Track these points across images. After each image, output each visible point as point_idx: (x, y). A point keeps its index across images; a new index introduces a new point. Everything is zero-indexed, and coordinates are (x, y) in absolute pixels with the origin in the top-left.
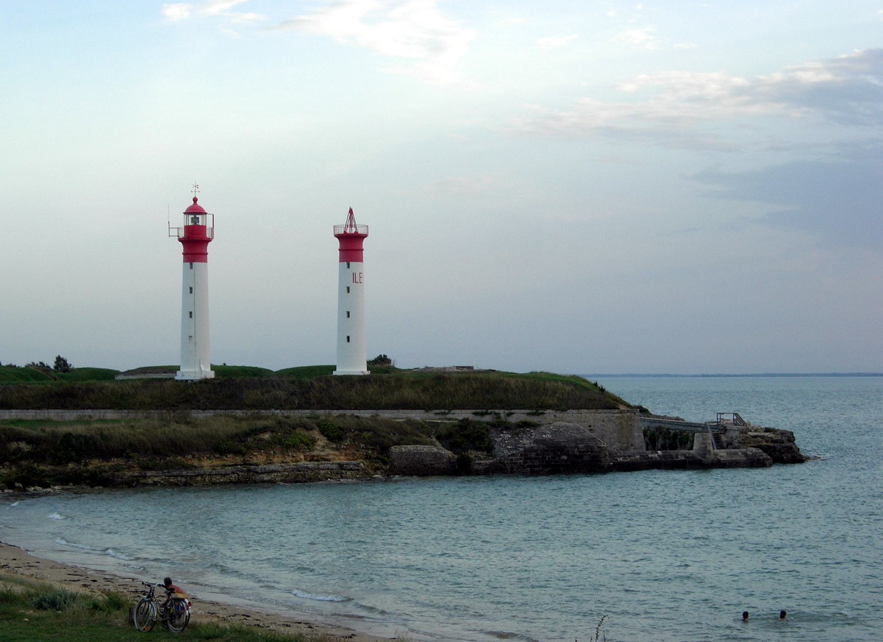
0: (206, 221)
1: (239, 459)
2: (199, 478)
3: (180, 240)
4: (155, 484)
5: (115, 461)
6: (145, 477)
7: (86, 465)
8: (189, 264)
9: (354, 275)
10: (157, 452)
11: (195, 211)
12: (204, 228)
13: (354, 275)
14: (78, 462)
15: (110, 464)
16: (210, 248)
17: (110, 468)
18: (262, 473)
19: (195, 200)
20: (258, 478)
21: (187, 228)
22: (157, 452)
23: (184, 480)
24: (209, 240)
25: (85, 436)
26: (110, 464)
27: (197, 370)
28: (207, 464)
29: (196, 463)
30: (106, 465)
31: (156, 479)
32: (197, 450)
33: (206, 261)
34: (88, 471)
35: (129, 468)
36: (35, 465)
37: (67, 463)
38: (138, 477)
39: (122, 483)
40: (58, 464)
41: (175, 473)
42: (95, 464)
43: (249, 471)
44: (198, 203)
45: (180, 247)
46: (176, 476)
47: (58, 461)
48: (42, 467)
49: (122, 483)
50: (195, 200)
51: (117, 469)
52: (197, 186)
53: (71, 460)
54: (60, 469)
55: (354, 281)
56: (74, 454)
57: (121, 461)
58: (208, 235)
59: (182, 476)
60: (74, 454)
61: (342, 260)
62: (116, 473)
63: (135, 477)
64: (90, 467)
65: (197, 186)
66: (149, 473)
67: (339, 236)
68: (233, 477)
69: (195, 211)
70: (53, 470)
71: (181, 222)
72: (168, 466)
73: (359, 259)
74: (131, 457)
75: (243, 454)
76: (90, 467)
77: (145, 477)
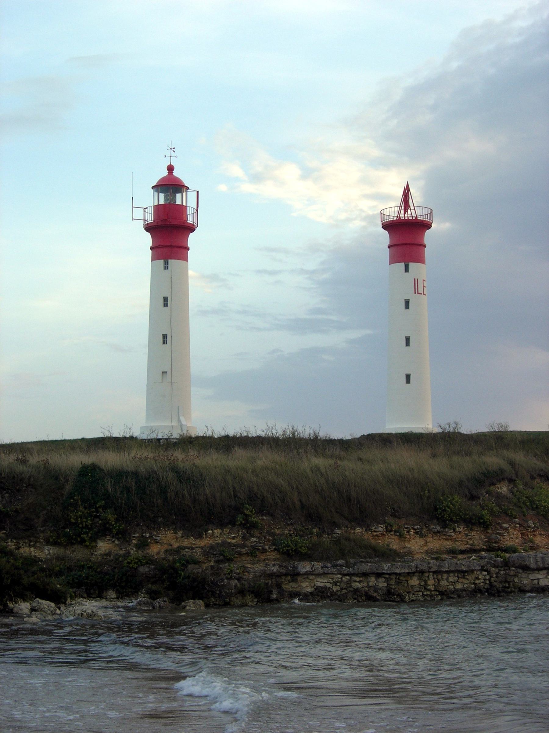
0: (187, 200)
1: (477, 538)
2: (415, 581)
3: (148, 228)
4: (320, 594)
5: (216, 536)
6: (295, 575)
7: (143, 544)
8: (162, 262)
9: (416, 282)
10: (313, 517)
11: (170, 185)
12: (182, 209)
13: (416, 282)
14: (122, 536)
15: (205, 542)
16: (192, 239)
17: (208, 552)
18: (539, 569)
19: (171, 169)
20: (526, 580)
21: (158, 209)
22: (313, 517)
23: (382, 584)
24: (191, 229)
25: (136, 474)
26: (205, 542)
27: (175, 424)
28: (419, 546)
29: (393, 543)
30: (195, 545)
31: (321, 582)
32: (393, 515)
33: (186, 259)
34: (149, 561)
35: (253, 552)
36: (11, 545)
37: (94, 539)
38: (279, 575)
39: (242, 592)
40: (71, 541)
41: (366, 567)
42: (166, 542)
43: (506, 564)
44: (175, 173)
45: (147, 239)
46: (365, 575)
47: (70, 534)
48: (26, 551)
49: (242, 592)
50: (171, 169)
51: (222, 554)
52: (172, 149)
53: (104, 531)
54: (78, 554)
55: (416, 291)
56: (110, 516)
57: (230, 536)
58: (190, 220)
59: (379, 575)
60: (110, 516)
61: (393, 260)
62: (225, 566)
63: (272, 575)
64: (154, 550)
65: (172, 149)
66: (305, 567)
67: (389, 226)
68: (482, 579)
69: (170, 185)
70: (58, 558)
71: (149, 200)
72: (342, 551)
73: (420, 259)
74: (254, 526)
75: (484, 525)
76: (154, 550)
77: (295, 575)
